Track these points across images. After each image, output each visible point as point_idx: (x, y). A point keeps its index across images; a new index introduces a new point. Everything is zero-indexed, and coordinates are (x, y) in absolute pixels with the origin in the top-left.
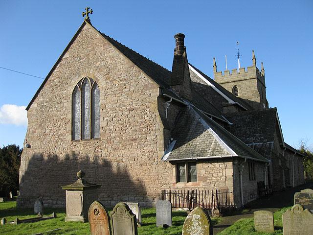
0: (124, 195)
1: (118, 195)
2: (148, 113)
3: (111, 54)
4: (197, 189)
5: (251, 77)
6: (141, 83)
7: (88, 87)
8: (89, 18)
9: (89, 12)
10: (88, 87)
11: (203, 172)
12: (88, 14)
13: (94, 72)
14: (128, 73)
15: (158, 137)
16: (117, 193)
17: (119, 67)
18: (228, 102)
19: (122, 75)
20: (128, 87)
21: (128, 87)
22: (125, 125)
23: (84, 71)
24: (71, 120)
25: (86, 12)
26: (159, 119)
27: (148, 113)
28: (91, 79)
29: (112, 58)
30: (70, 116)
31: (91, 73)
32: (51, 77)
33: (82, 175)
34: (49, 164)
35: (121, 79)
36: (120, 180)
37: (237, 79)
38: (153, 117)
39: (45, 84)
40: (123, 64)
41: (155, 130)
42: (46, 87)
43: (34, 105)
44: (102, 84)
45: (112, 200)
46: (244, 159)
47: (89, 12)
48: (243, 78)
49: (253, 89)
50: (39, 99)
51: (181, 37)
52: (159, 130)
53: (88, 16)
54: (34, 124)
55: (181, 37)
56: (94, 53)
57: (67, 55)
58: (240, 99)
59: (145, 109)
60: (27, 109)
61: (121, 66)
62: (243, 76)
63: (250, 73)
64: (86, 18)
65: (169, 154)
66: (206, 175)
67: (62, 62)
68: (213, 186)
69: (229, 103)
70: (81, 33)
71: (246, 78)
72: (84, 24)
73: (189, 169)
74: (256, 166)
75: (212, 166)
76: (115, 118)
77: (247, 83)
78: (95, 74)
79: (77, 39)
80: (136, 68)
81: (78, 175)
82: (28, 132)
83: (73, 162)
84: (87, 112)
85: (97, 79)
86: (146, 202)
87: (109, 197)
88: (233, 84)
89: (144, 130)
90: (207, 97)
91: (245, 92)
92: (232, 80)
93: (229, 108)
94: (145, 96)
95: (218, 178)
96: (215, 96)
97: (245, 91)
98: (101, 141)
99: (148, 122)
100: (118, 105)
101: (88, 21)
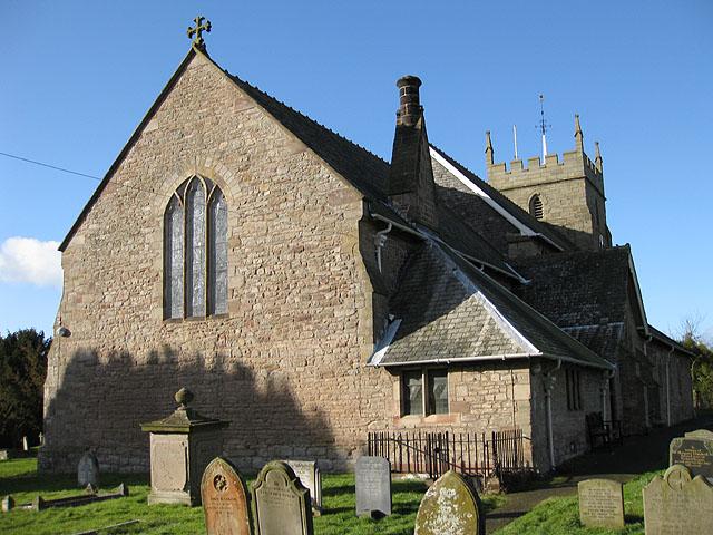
0: (283, 444)
1: (269, 445)
2: (338, 257)
3: (252, 123)
4: (450, 430)
5: (572, 175)
6: (322, 188)
7: (201, 197)
8: (202, 41)
9: (203, 26)
10: (201, 197)
11: (462, 391)
12: (200, 31)
13: (214, 163)
14: (291, 165)
15: (360, 311)
16: (266, 440)
17: (271, 153)
18: (519, 231)
19: (279, 172)
20: (291, 198)
21: (291, 198)
22: (285, 285)
23: (192, 162)
24: (161, 274)
25: (195, 27)
26: (361, 271)
27: (338, 257)
28: (207, 180)
29: (255, 131)
30: (159, 264)
31: (208, 166)
32: (116, 175)
33: (188, 397)
34: (113, 374)
35: (275, 179)
36: (272, 409)
37: (540, 180)
38: (349, 266)
39: (103, 192)
40: (279, 147)
41: (354, 296)
42: (104, 197)
43: (78, 239)
44: (231, 192)
45: (256, 455)
46: (556, 362)
47: (203, 26)
48: (553, 178)
49: (576, 202)
50: (90, 225)
51: (412, 85)
52: (363, 295)
53: (200, 36)
54: (76, 283)
55: (412, 85)
56: (215, 121)
57: (152, 126)
58: (546, 224)
59: (330, 248)
60: (62, 249)
61: (276, 149)
62: (553, 174)
63: (568, 165)
64: (196, 40)
65: (385, 350)
66: (469, 399)
67: (141, 142)
68: (485, 424)
69: (523, 234)
70: (185, 74)
71: (560, 177)
72: (192, 54)
73: (430, 384)
74: (584, 379)
75: (484, 379)
76: (262, 269)
77: (564, 188)
78: (217, 169)
79: (176, 89)
80: (309, 155)
81: (178, 397)
82: (65, 300)
83: (167, 369)
84: (199, 255)
85: (221, 179)
86: (333, 459)
87: (248, 447)
88: (530, 192)
89: (328, 296)
90: (472, 222)
91: (558, 210)
92: (528, 183)
93: (521, 245)
94: (330, 219)
95: (495, 406)
96: (491, 219)
97: (558, 207)
98: (231, 322)
99: (337, 278)
100: (269, 238)
101: (202, 47)
